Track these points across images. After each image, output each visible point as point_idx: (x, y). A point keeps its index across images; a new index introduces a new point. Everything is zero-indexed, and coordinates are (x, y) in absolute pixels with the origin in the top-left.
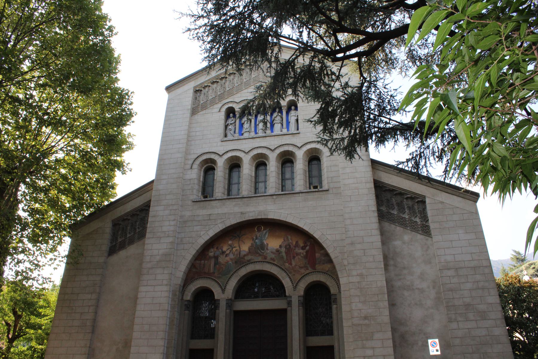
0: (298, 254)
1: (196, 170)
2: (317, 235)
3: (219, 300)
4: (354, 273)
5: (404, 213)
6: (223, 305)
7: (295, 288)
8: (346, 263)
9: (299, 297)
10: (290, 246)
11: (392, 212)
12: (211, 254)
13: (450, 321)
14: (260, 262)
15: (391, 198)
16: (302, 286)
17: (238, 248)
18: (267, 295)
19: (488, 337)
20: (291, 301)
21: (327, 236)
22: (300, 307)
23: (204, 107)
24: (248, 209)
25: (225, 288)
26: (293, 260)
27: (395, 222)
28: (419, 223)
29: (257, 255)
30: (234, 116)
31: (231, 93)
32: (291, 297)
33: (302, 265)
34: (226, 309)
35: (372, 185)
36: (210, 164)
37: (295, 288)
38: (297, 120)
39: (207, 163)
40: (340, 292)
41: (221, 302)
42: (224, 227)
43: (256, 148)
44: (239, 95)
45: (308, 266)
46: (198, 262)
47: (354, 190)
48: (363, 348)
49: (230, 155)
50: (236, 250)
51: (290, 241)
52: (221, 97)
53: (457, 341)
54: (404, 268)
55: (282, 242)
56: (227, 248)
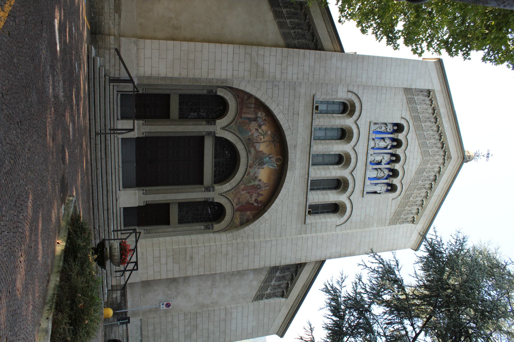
0: (251, 196)
1: (346, 97)
2: (266, 215)
3: (215, 125)
4: (230, 249)
5: (276, 281)
6: (210, 128)
7: (221, 194)
8: (239, 240)
9: (213, 198)
10: (259, 189)
11: (278, 272)
12: (259, 114)
13: (185, 315)
14: (248, 162)
15: (290, 271)
16: (223, 201)
17: (263, 140)
18: (216, 165)
19: (172, 339)
20: (210, 191)
21: (264, 224)
22: (204, 199)
23: (410, 101)
24: (298, 152)
25: (225, 130)
26: (246, 192)
27: (269, 275)
28: (266, 292)
29: (254, 159)
30: (393, 147)
31: (418, 128)
32: (213, 191)
33: (240, 200)
34: (206, 132)
35: (303, 261)
36: (349, 108)
37: (221, 194)
38: (375, 193)
39: (351, 107)
40: (214, 232)
41: (212, 126)
42: (284, 129)
43: (357, 157)
44: (414, 136)
45: (240, 205)
46: (253, 101)
47: (301, 247)
48: (167, 256)
49: (355, 131)
50: (261, 139)
51: (264, 189)
52: (416, 119)
53: (169, 319)
54: (230, 282)
55: (264, 182)
56: (264, 130)
